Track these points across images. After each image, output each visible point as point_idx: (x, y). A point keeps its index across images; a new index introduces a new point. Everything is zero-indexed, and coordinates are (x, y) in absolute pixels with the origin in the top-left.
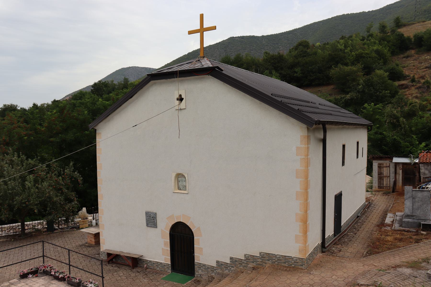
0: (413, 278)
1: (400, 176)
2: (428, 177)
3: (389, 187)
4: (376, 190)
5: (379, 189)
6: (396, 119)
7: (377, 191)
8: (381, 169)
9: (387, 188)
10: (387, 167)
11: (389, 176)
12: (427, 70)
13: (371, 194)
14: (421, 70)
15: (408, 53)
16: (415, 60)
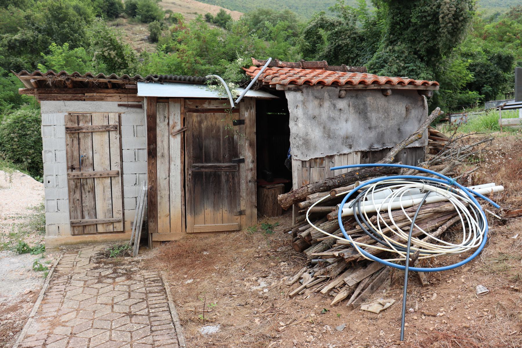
0: (143, 339)
1: (172, 166)
2: (322, 159)
3: (119, 222)
4: (63, 242)
5: (74, 235)
6: (116, 51)
7: (66, 244)
8: (82, 141)
9: (111, 228)
10: (107, 129)
11: (121, 173)
12: (142, 43)
13: (34, 270)
14: (135, 41)
15: (119, 20)
16: (128, 29)
